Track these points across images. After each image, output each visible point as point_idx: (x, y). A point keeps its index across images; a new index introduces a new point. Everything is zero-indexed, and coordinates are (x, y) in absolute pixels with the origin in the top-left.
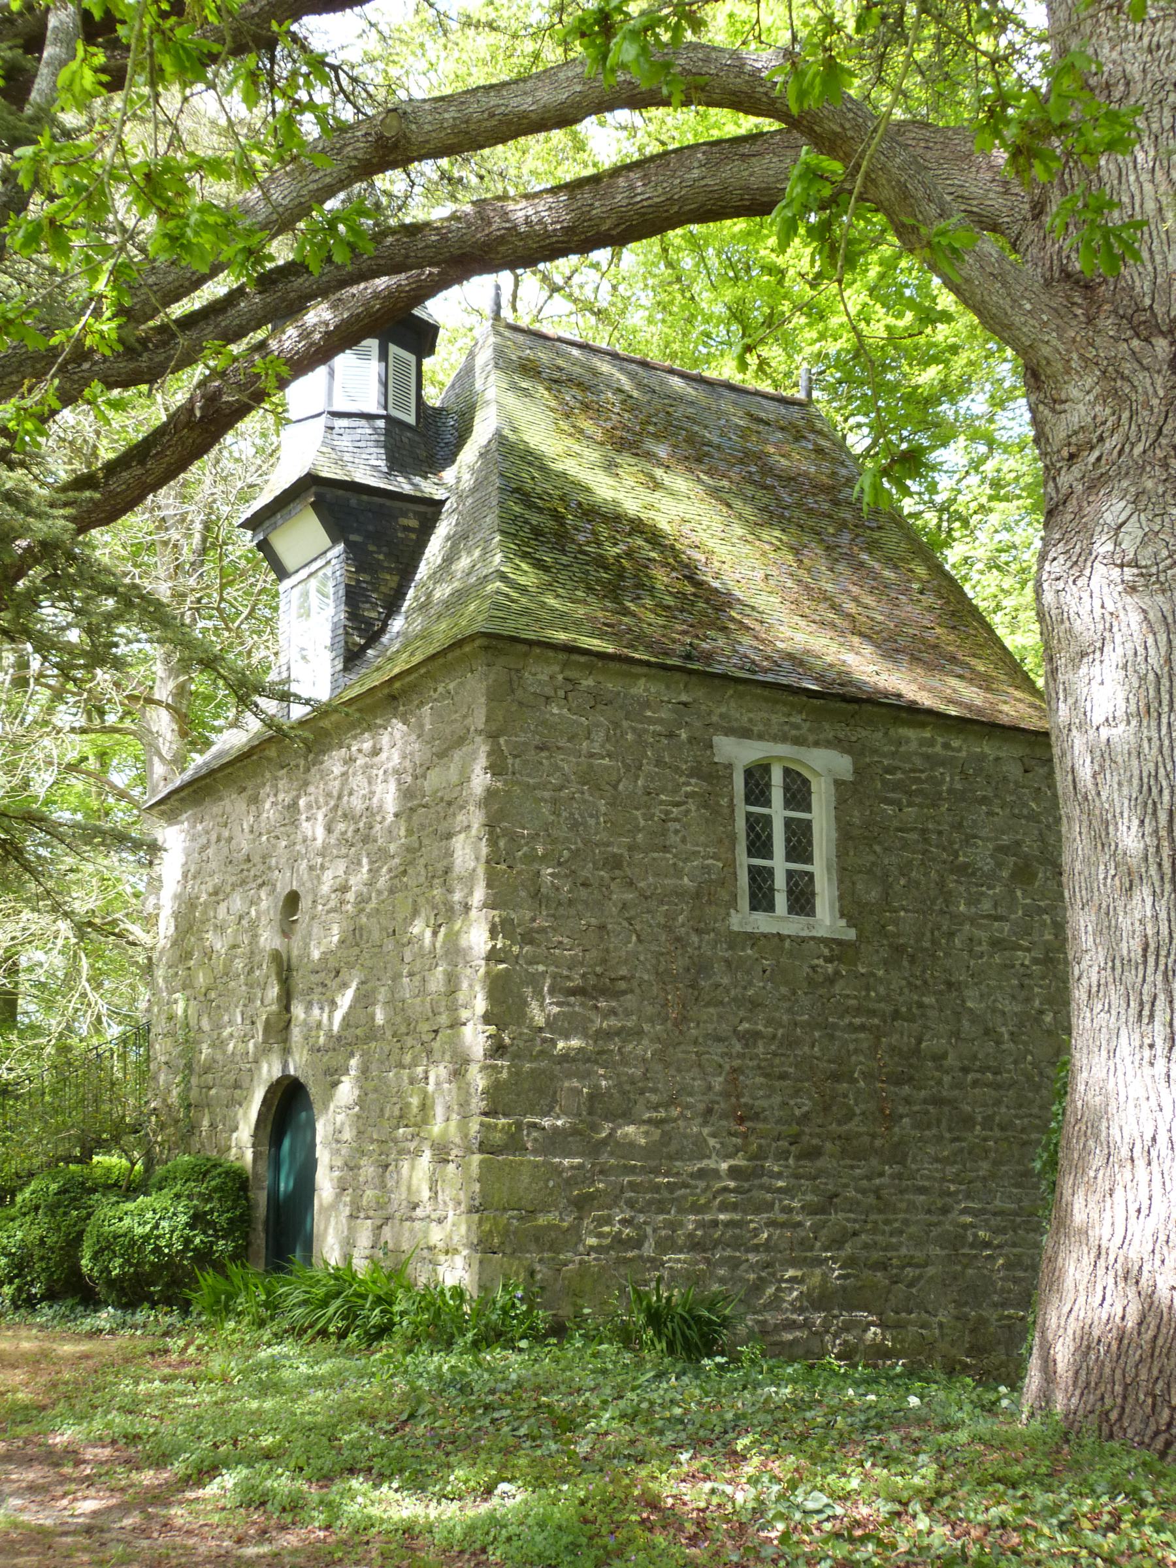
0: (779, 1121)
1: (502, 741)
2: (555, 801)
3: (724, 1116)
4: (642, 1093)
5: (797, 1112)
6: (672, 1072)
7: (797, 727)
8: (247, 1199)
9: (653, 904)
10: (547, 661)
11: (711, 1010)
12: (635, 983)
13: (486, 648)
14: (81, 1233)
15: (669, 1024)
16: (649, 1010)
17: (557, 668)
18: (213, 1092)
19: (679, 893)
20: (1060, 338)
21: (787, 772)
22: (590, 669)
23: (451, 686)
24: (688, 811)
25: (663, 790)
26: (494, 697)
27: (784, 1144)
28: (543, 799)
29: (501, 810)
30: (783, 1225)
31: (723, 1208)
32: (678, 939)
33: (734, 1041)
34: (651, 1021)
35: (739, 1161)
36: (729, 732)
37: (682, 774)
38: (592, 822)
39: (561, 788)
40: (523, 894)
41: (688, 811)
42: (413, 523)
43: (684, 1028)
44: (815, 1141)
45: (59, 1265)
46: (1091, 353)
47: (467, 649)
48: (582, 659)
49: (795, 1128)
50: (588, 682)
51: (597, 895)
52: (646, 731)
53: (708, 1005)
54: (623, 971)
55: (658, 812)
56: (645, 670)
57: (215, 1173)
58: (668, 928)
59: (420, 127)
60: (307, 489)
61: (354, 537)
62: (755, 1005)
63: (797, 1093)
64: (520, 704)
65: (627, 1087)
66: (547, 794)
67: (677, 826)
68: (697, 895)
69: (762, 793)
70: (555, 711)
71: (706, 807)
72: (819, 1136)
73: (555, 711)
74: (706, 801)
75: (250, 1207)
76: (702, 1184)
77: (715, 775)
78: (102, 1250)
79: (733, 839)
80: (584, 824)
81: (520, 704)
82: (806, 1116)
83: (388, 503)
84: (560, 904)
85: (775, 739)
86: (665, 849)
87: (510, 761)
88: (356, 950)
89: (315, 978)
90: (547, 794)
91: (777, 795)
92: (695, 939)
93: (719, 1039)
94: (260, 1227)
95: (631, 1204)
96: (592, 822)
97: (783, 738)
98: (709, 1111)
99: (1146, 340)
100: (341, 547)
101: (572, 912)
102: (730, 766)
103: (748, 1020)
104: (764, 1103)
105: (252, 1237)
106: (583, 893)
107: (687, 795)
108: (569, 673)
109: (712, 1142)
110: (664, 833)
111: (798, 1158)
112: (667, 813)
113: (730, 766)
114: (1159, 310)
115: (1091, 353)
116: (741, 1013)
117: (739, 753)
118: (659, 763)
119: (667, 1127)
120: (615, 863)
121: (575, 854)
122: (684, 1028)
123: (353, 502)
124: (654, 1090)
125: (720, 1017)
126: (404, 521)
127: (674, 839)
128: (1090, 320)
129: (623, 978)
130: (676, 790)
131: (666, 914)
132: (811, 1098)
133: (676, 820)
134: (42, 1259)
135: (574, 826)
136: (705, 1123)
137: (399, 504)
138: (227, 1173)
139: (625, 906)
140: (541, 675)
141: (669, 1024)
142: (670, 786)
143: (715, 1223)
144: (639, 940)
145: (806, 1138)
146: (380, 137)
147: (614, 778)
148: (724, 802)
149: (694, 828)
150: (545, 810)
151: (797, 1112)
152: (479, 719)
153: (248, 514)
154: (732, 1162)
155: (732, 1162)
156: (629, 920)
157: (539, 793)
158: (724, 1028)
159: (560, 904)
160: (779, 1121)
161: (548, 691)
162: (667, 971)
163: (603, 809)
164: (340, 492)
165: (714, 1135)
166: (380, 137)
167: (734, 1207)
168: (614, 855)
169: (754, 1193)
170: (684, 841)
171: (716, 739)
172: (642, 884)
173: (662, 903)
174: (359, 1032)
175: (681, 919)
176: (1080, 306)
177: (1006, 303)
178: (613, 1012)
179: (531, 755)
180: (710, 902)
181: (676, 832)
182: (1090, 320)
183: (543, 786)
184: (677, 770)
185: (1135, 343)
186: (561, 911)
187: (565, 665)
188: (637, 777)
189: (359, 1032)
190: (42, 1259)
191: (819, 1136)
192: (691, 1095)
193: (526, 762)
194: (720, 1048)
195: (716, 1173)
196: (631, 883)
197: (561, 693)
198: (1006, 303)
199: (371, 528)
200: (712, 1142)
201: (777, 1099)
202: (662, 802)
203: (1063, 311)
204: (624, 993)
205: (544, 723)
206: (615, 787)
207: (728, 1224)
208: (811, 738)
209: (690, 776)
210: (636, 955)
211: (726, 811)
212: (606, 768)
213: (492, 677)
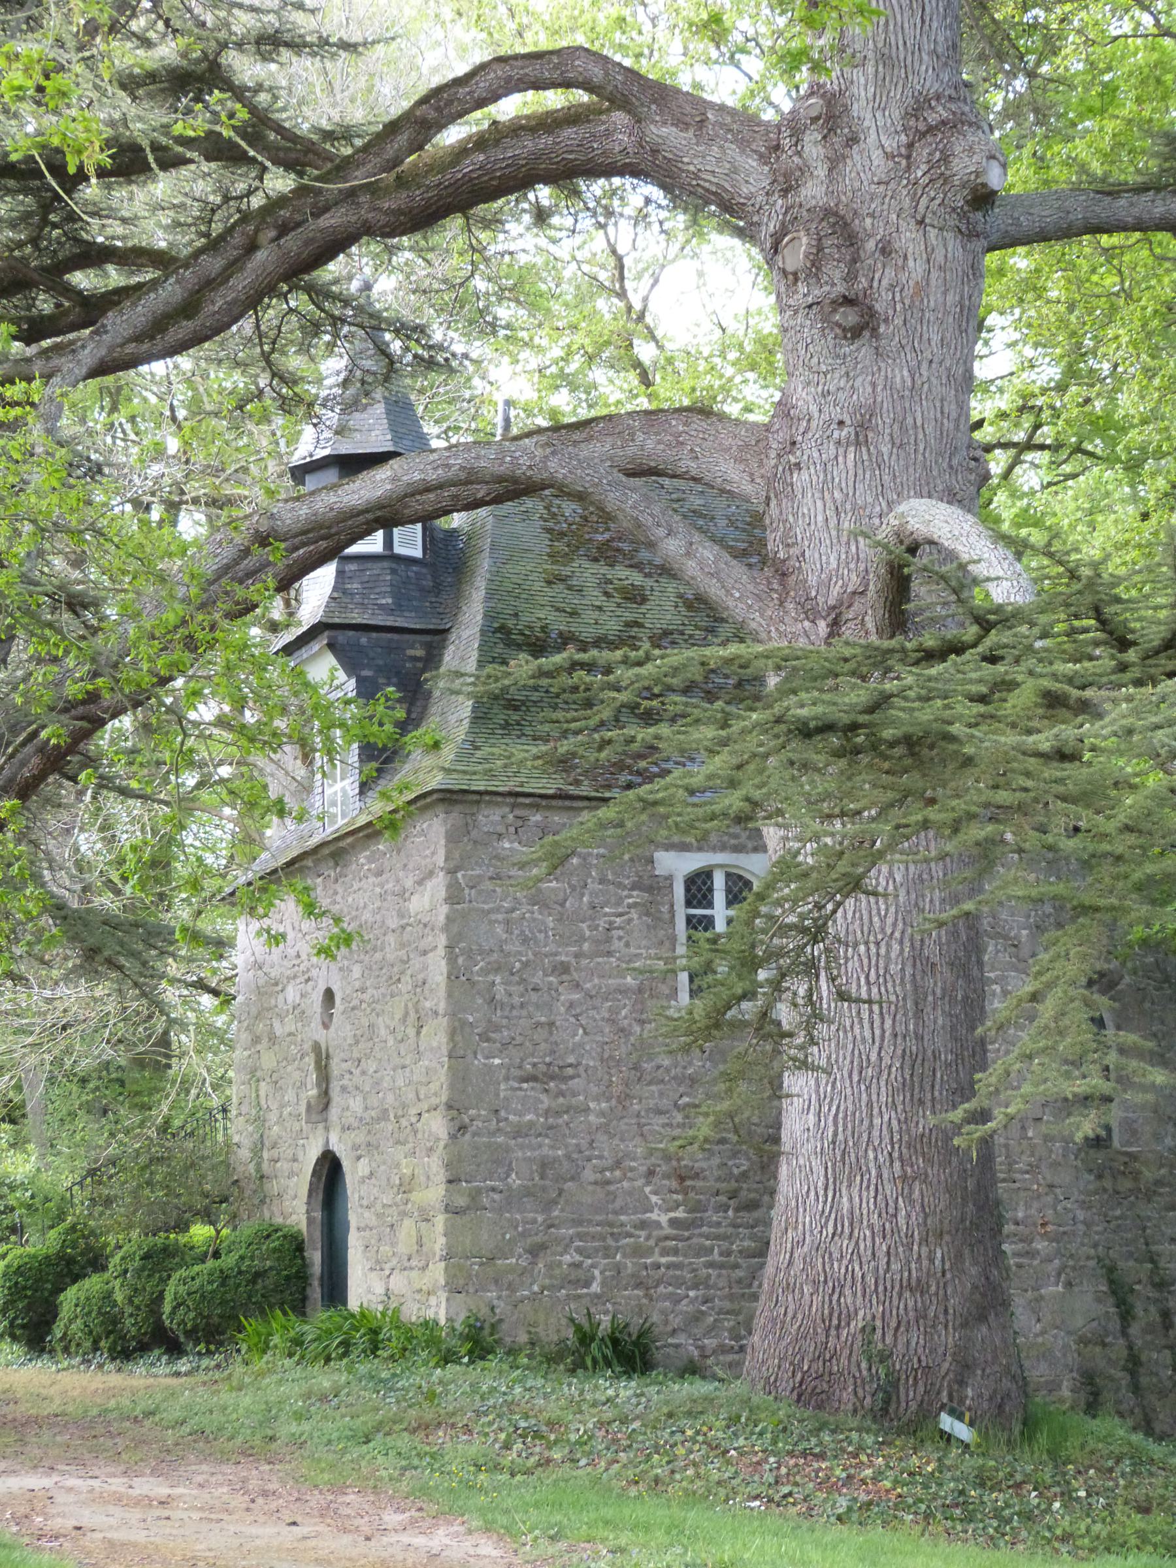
0: (719, 1179)
1: (459, 875)
2: (507, 922)
3: (667, 1176)
4: (589, 1160)
5: (736, 1171)
6: (616, 1141)
7: (736, 836)
8: (303, 1258)
9: (597, 1002)
10: (497, 804)
11: (653, 1088)
12: (581, 1069)
13: (442, 800)
14: (162, 1292)
15: (614, 1102)
16: (594, 1089)
17: (507, 810)
18: (279, 1165)
19: (623, 991)
20: (762, 616)
21: (728, 875)
22: (537, 807)
23: (425, 826)
24: (630, 921)
25: (606, 904)
26: (452, 839)
27: (723, 1199)
28: (496, 921)
29: (460, 934)
30: (722, 1266)
31: (665, 1252)
32: (622, 1030)
33: (675, 1113)
34: (597, 1099)
35: (680, 1214)
36: (669, 847)
37: (624, 888)
38: (541, 936)
39: (513, 910)
40: (480, 1001)
41: (630, 921)
42: (420, 653)
43: (627, 1104)
44: (752, 1195)
45: (145, 1320)
46: (782, 628)
47: (428, 800)
48: (527, 801)
49: (734, 1185)
50: (538, 818)
51: (546, 997)
52: (590, 854)
53: (650, 1083)
54: (571, 1060)
55: (602, 923)
56: (586, 803)
57: (274, 1236)
58: (612, 1021)
59: (283, 522)
60: (322, 632)
61: (366, 673)
62: (693, 1081)
63: (735, 1154)
64: (475, 842)
65: (575, 1156)
66: (500, 917)
67: (621, 933)
68: (640, 990)
69: (705, 897)
70: (507, 845)
71: (648, 914)
72: (756, 1191)
73: (507, 845)
74: (647, 910)
75: (305, 1265)
76: (643, 1233)
77: (657, 887)
78: (179, 1305)
79: (673, 939)
80: (535, 939)
81: (475, 842)
82: (744, 1175)
83: (396, 636)
84: (513, 1007)
85: (714, 849)
86: (609, 954)
87: (467, 891)
88: (370, 1044)
89: (345, 1066)
90: (500, 917)
91: (719, 897)
92: (637, 1029)
93: (660, 1112)
94: (316, 1283)
95: (579, 1251)
96: (541, 936)
97: (723, 848)
98: (651, 1173)
99: (813, 622)
100: (353, 681)
101: (524, 1013)
102: (670, 878)
103: (687, 1094)
104: (704, 1165)
105: (309, 1291)
106: (534, 997)
107: (629, 906)
108: (518, 812)
109: (654, 1199)
110: (608, 940)
111: (737, 1210)
112: (611, 923)
113: (670, 878)
114: (821, 600)
115: (782, 628)
116: (681, 1090)
117: (677, 865)
118: (602, 881)
119: (612, 1188)
120: (564, 969)
121: (526, 965)
122: (627, 1104)
123: (364, 640)
124: (600, 1157)
125: (661, 1094)
126: (411, 652)
127: (617, 945)
128: (781, 604)
129: (570, 1065)
130: (619, 903)
131: (610, 1009)
132: (749, 1159)
133: (618, 928)
134: (131, 1315)
135: (525, 941)
136: (648, 1183)
137: (407, 637)
138: (285, 1237)
139: (571, 1005)
140: (491, 817)
141: (614, 1102)
142: (613, 900)
143: (658, 1266)
144: (585, 1033)
145: (743, 1193)
146: (257, 531)
147: (561, 896)
148: (665, 909)
149: (636, 934)
150: (499, 930)
151: (736, 1171)
152: (440, 859)
153: (279, 646)
154: (672, 1215)
155: (672, 1215)
156: (576, 1016)
157: (493, 917)
158: (665, 1103)
159: (513, 1007)
160: (719, 1179)
161: (501, 829)
162: (611, 1057)
163: (551, 925)
164: (351, 633)
165: (655, 1193)
166: (257, 531)
167: (676, 1251)
168: (562, 963)
169: (695, 1240)
170: (627, 945)
171: (657, 855)
172: (588, 985)
173: (607, 999)
174: (373, 1113)
175: (623, 1013)
176: (776, 591)
177: (722, 593)
178: (562, 1094)
179: (488, 885)
180: (651, 996)
181: (620, 938)
182: (781, 604)
183: (498, 910)
184: (620, 885)
185: (806, 624)
186: (515, 1013)
187: (514, 806)
188: (583, 895)
189: (373, 1113)
190: (131, 1315)
191: (756, 1191)
192: (634, 1159)
193: (480, 893)
194: (663, 1120)
195: (658, 1225)
196: (578, 985)
197: (512, 830)
198: (722, 593)
199: (381, 662)
200: (654, 1199)
201: (716, 1161)
202: (606, 915)
203: (764, 596)
204: (572, 1077)
205: (497, 857)
206: (562, 905)
207: (669, 1266)
208: (750, 845)
209: (632, 889)
210: (581, 1045)
211: (667, 916)
212: (553, 890)
213: (450, 823)
